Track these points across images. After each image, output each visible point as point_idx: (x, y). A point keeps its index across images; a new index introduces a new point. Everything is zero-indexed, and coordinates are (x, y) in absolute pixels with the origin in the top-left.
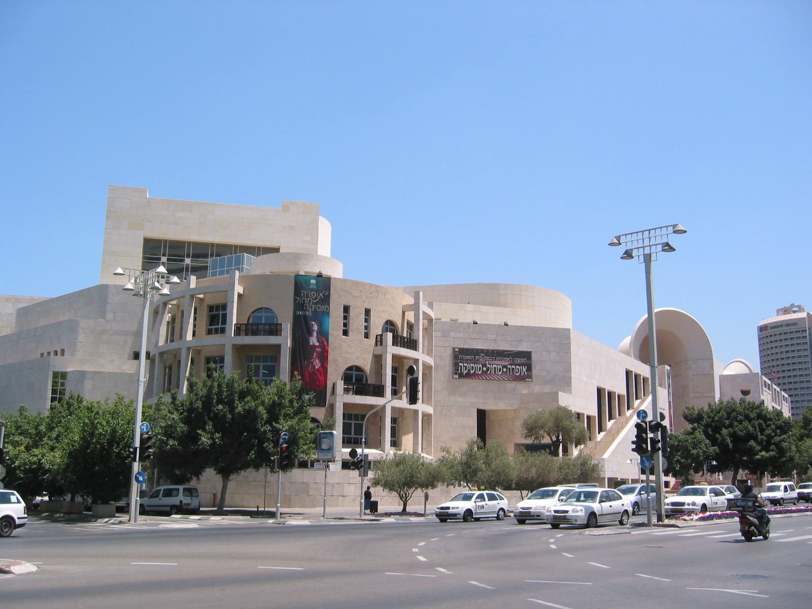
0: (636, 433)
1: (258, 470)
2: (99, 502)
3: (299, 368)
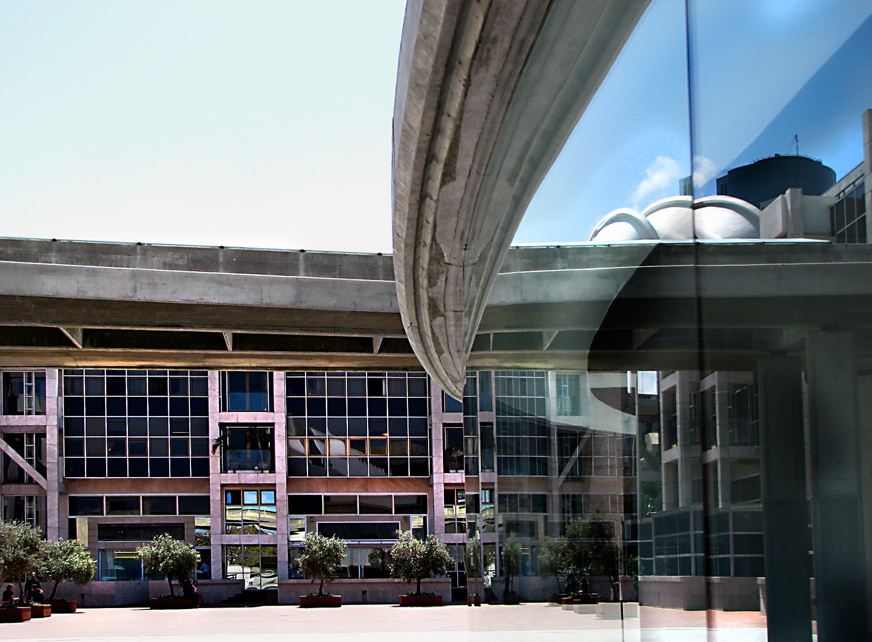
1: (776, 155)
3: (205, 370)
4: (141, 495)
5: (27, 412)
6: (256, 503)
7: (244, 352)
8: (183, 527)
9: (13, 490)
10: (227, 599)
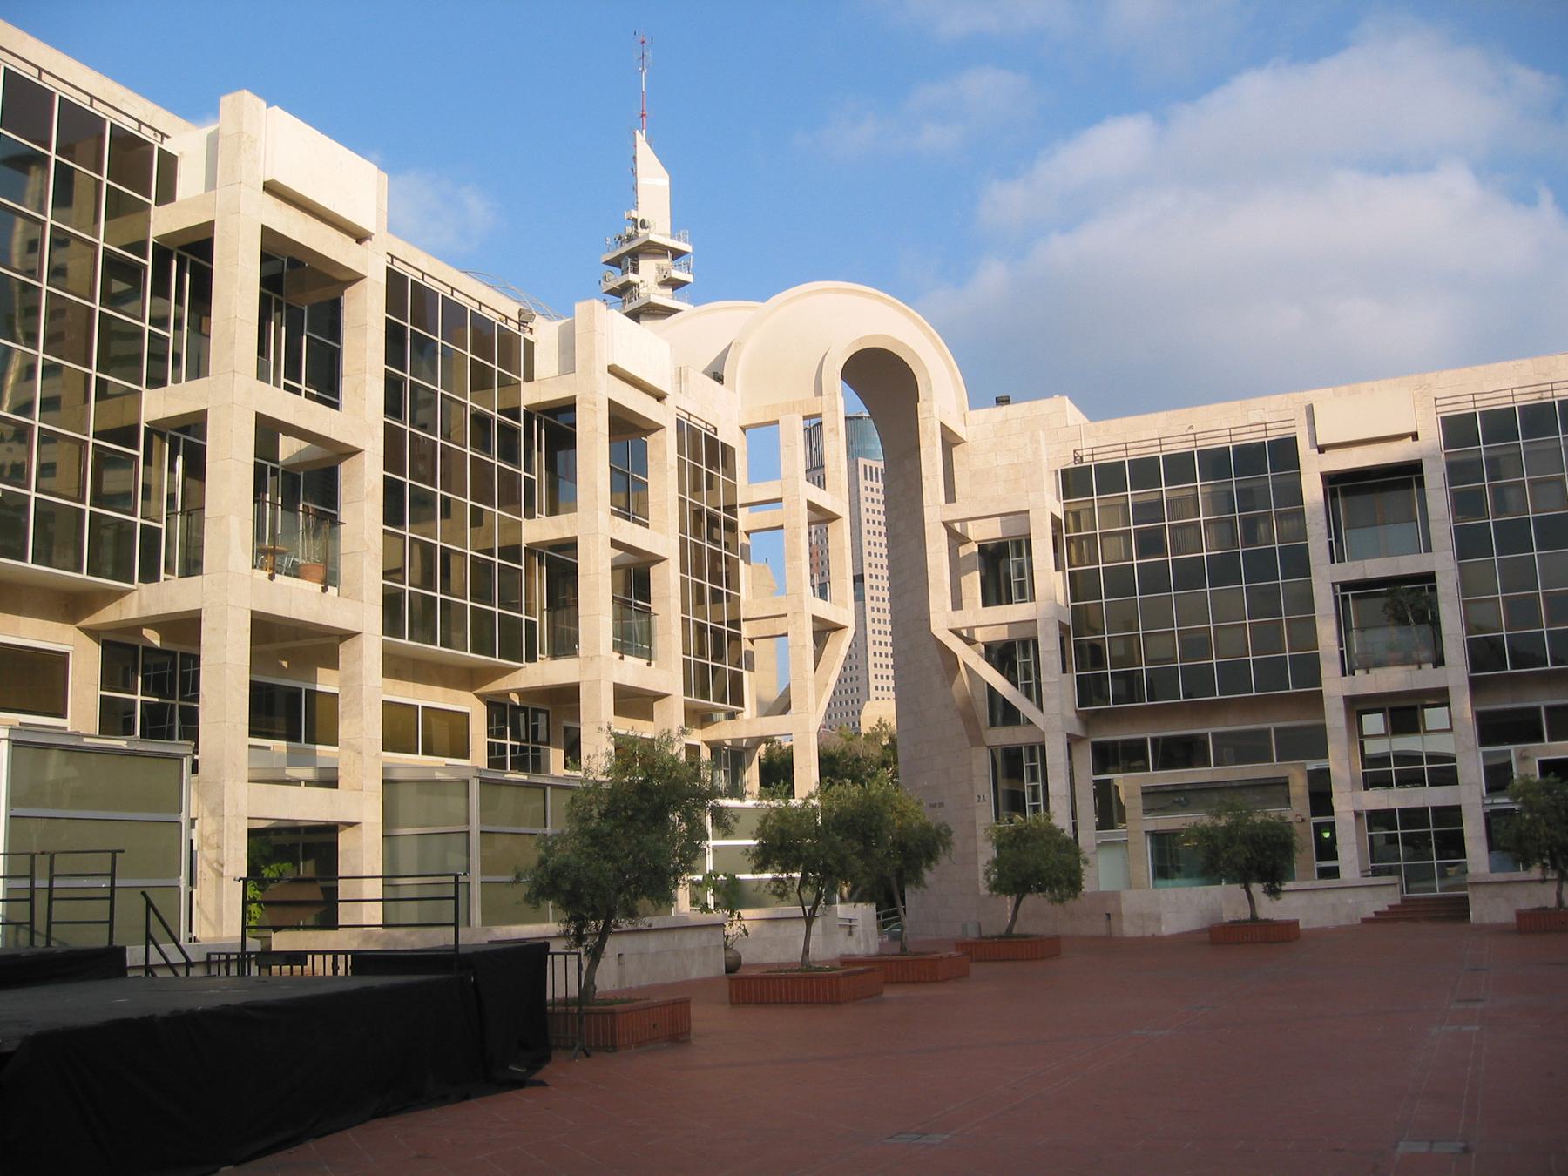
2: (745, 741)
4: (1210, 731)
6: (1383, 732)
7: (419, 954)
8: (1287, 784)
9: (1005, 736)
10: (1373, 915)
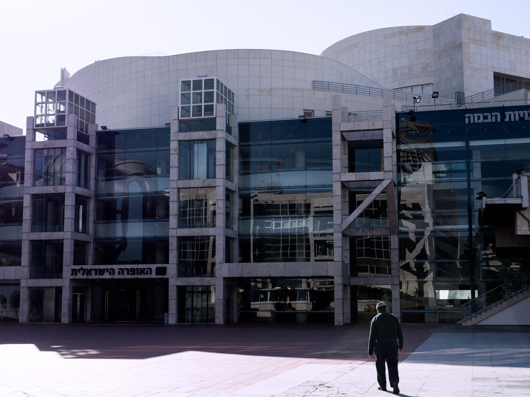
0: (30, 349)
2: (369, 141)
5: (160, 212)
